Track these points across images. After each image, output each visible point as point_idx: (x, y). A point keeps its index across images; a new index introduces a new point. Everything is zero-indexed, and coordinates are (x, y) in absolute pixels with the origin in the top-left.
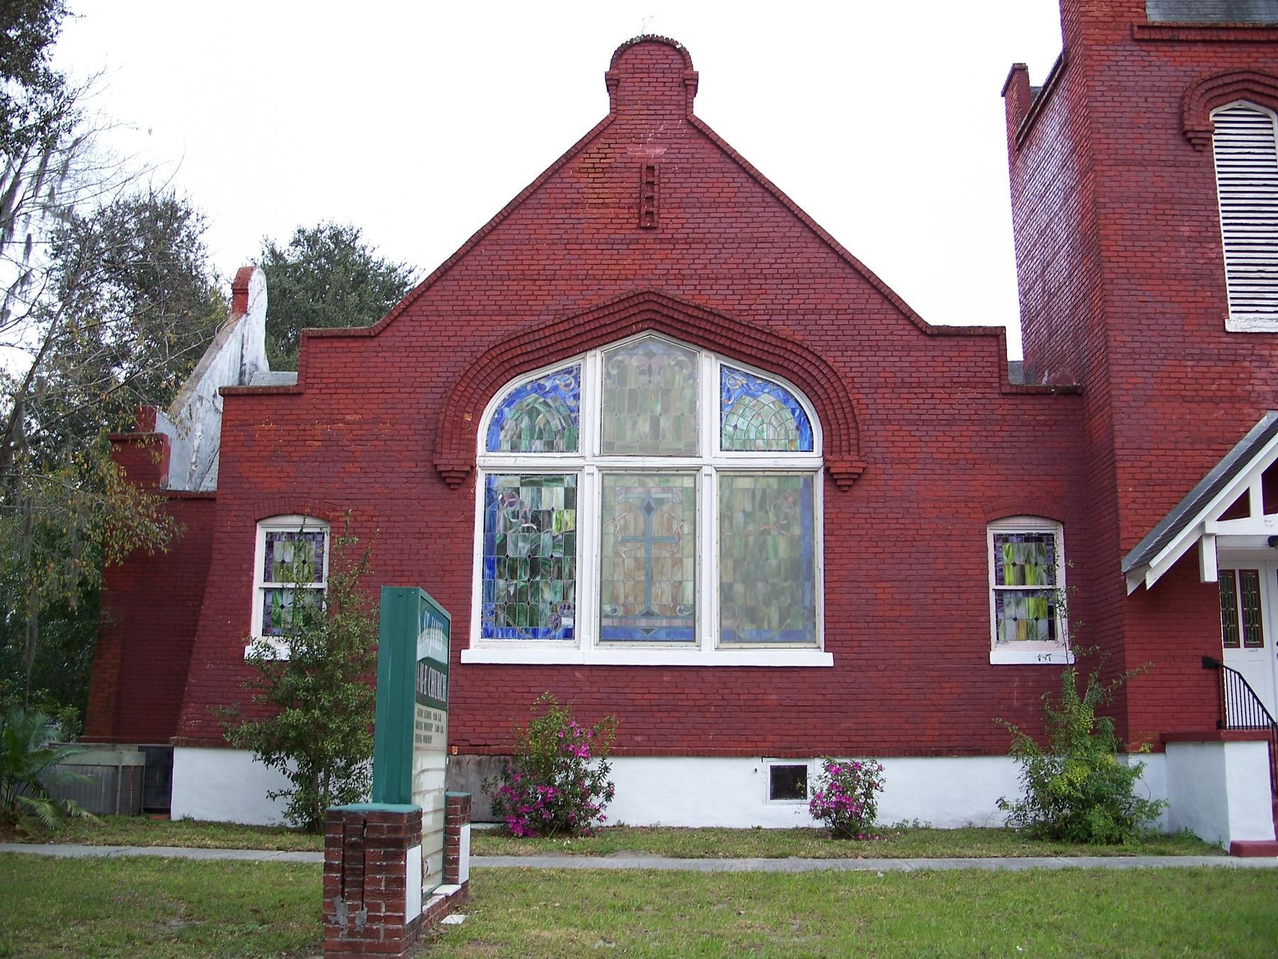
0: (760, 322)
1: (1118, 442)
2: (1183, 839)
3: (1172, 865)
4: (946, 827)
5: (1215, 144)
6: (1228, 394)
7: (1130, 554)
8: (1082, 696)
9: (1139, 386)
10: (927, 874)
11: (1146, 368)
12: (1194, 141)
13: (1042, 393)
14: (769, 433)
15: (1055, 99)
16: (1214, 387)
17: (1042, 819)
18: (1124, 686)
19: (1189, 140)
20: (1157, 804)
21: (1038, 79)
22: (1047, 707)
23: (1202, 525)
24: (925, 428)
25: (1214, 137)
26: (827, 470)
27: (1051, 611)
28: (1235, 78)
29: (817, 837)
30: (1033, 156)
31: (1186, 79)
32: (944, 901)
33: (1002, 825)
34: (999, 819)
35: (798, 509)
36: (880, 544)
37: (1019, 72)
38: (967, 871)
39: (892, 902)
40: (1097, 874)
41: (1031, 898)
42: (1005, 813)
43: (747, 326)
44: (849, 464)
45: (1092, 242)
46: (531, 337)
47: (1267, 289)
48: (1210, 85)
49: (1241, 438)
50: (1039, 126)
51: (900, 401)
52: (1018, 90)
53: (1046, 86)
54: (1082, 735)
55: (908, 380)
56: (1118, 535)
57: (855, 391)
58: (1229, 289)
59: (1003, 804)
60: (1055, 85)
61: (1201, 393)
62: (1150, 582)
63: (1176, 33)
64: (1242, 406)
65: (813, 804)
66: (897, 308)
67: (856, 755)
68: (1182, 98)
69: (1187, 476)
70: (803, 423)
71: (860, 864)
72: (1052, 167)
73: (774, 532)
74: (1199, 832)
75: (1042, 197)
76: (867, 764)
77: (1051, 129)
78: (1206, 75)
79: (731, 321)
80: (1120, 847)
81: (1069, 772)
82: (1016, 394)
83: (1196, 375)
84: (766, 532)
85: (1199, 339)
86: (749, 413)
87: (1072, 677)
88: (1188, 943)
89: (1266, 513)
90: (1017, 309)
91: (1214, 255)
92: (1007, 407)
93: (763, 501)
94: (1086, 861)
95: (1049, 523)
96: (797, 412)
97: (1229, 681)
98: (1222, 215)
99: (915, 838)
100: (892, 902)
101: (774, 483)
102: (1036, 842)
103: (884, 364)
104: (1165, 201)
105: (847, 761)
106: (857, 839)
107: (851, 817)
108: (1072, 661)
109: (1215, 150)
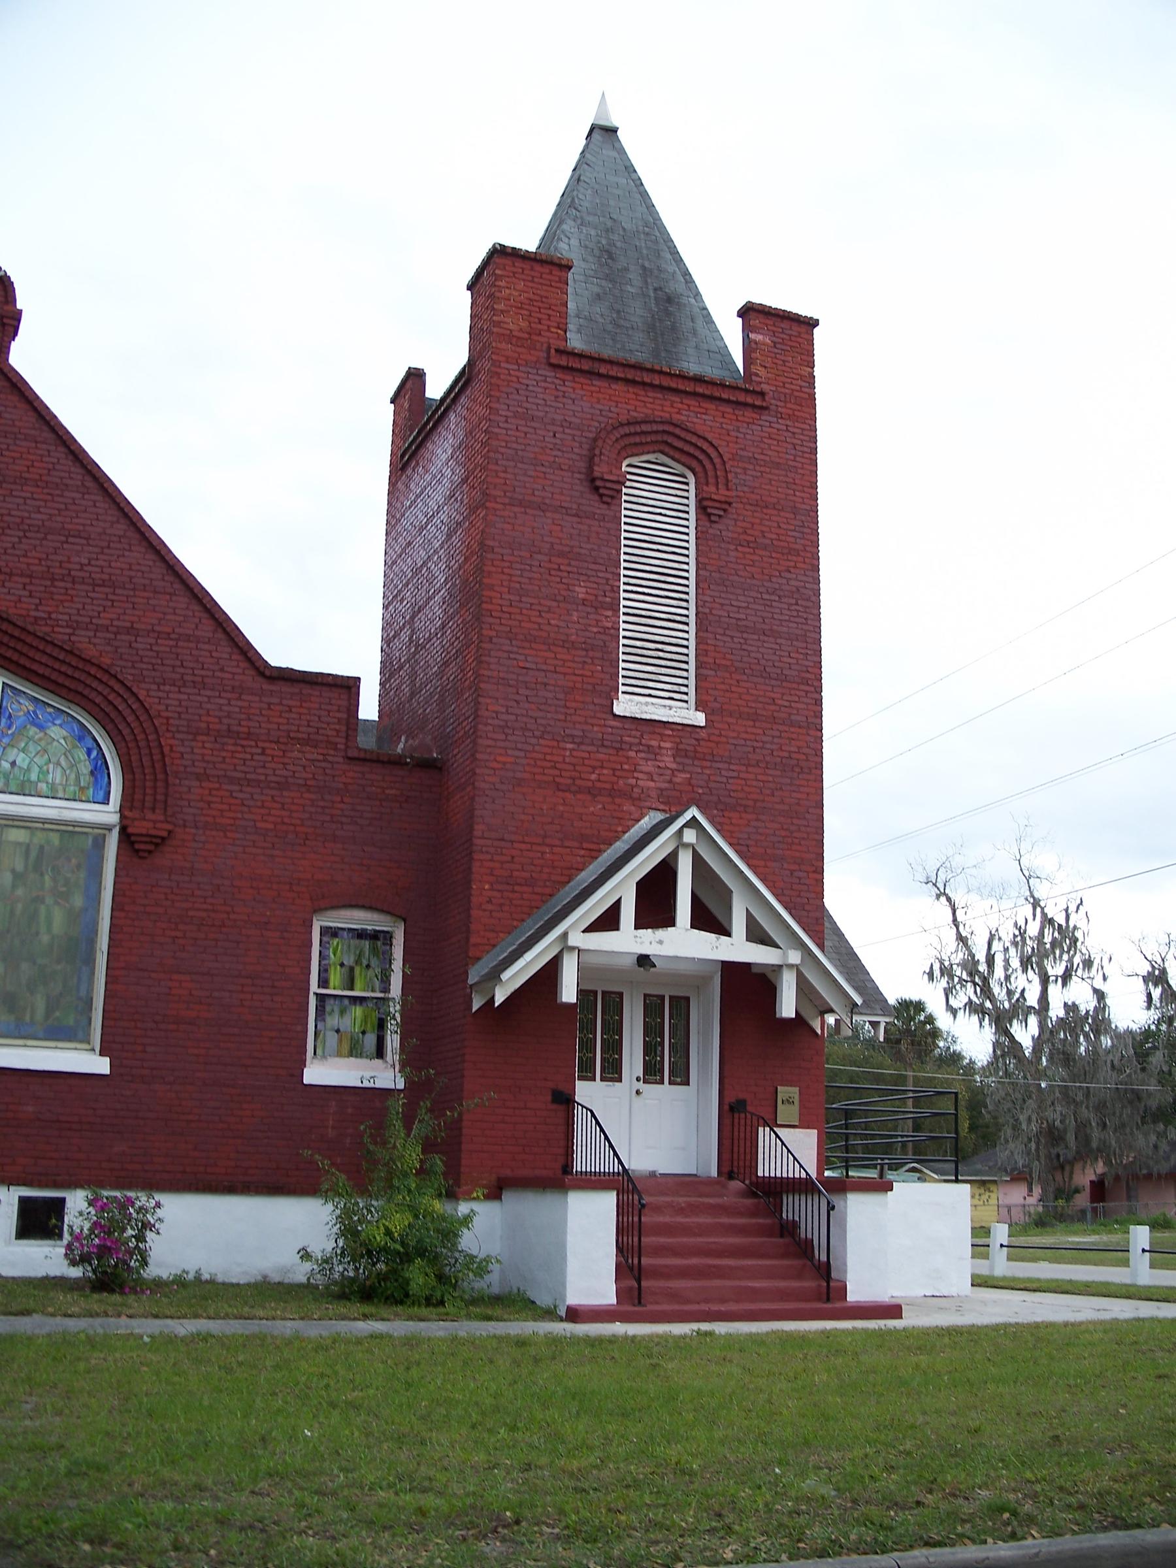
0: (61, 635)
1: (479, 829)
2: (515, 1302)
3: (498, 1332)
4: (234, 1281)
5: (624, 498)
6: (608, 786)
7: (481, 963)
8: (408, 1128)
9: (508, 766)
10: (205, 1340)
11: (519, 746)
12: (601, 491)
13: (397, 762)
14: (55, 776)
15: (452, 416)
16: (593, 777)
17: (351, 1274)
18: (460, 1119)
19: (597, 489)
20: (487, 1259)
21: (435, 389)
22: (366, 1139)
23: (565, 935)
24: (249, 789)
25: (624, 490)
26: (123, 830)
27: (381, 1025)
28: (655, 427)
29: (72, 1289)
30: (418, 480)
31: (601, 419)
32: (223, 1373)
33: (304, 1280)
34: (301, 1272)
35: (82, 875)
36: (181, 927)
37: (415, 378)
38: (254, 1336)
39: (158, 1374)
40: (411, 1342)
41: (329, 1371)
42: (308, 1266)
43: (43, 639)
44: (151, 825)
45: (473, 590)
46: (105, 678)
47: (664, 671)
48: (626, 430)
49: (618, 838)
50: (429, 445)
51: (224, 754)
52: (410, 399)
53: (443, 399)
54: (406, 1175)
55: (235, 728)
56: (467, 939)
57: (169, 735)
58: (622, 665)
59: (305, 1255)
60: (454, 400)
61: (578, 782)
62: (499, 999)
63: (596, 365)
64: (621, 802)
65: (69, 1247)
66: (232, 639)
67: (130, 1187)
68: (595, 440)
69: (554, 878)
70: (100, 769)
71: (122, 1325)
72: (438, 496)
73: (49, 900)
74: (532, 1294)
75: (422, 529)
76: (142, 1199)
77: (443, 451)
78: (623, 419)
79: (23, 629)
80: (441, 1310)
81: (386, 1219)
82: (364, 760)
83: (574, 761)
84: (39, 900)
85: (582, 719)
86: (32, 748)
87: (397, 1106)
88: (505, 1424)
89: (636, 928)
90: (376, 658)
91: (610, 625)
92: (351, 774)
93: (38, 860)
94: (398, 1327)
95: (388, 918)
96: (94, 754)
97: (581, 1118)
98: (623, 579)
99: (196, 1293)
100: (158, 1374)
101: (55, 839)
102: (344, 1302)
103: (209, 706)
104: (561, 554)
105: (118, 1194)
106: (122, 1293)
107: (116, 1265)
108: (401, 1085)
109: (624, 505)
